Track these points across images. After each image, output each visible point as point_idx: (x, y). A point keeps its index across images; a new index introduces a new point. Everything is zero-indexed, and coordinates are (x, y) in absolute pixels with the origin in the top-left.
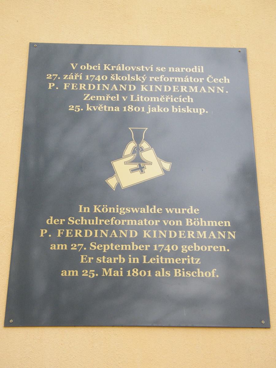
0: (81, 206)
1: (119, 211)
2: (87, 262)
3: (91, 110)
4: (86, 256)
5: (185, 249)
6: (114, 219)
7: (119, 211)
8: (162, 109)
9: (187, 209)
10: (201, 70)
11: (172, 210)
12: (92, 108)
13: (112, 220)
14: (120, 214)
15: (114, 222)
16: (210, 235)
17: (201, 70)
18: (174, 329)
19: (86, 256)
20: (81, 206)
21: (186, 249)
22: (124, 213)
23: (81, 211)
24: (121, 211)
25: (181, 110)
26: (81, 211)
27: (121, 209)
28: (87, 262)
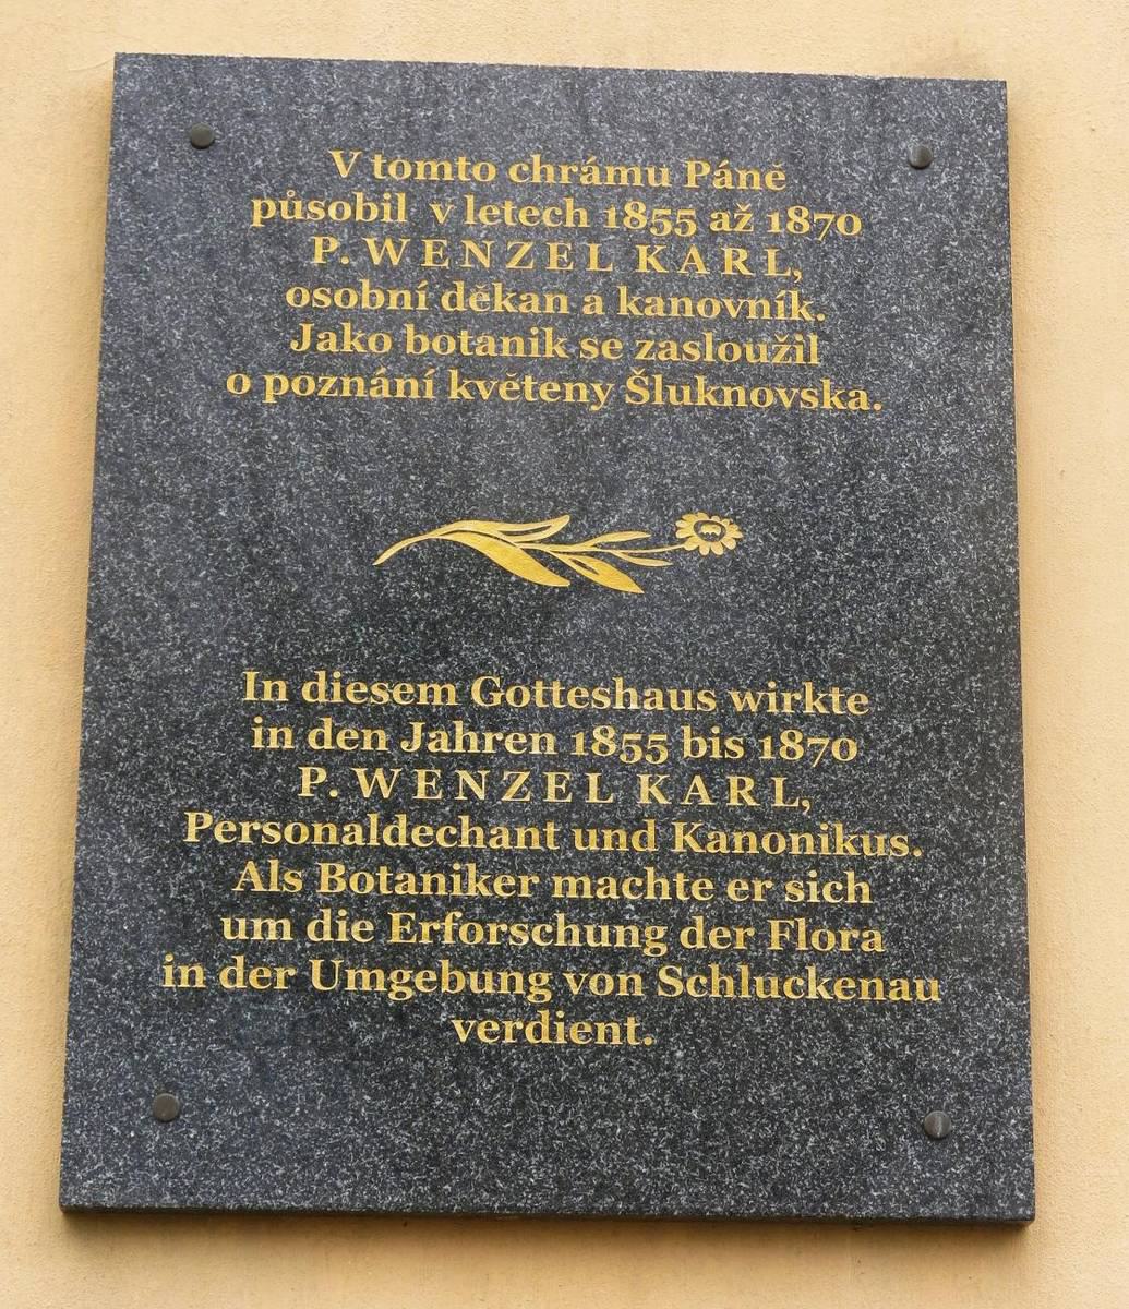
0: (251, 676)
1: (388, 985)
2: (413, 940)
3: (467, 395)
4: (413, 916)
5: (541, 988)
6: (454, 919)
7: (388, 985)
8: (485, 883)
9: (525, 1024)
10: (394, 215)
11: (755, 698)
12: (473, 389)
13: (449, 925)
14: (392, 996)
15: (455, 933)
16: (690, 793)
17: (394, 215)
18: (326, 1254)
19: (413, 916)
20: (251, 676)
21: (544, 987)
22: (409, 993)
23: (250, 696)
24: (393, 987)
25: (723, 749)
26: (250, 696)
27: (394, 975)
28: (413, 940)
